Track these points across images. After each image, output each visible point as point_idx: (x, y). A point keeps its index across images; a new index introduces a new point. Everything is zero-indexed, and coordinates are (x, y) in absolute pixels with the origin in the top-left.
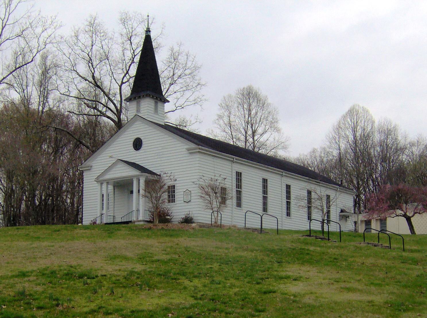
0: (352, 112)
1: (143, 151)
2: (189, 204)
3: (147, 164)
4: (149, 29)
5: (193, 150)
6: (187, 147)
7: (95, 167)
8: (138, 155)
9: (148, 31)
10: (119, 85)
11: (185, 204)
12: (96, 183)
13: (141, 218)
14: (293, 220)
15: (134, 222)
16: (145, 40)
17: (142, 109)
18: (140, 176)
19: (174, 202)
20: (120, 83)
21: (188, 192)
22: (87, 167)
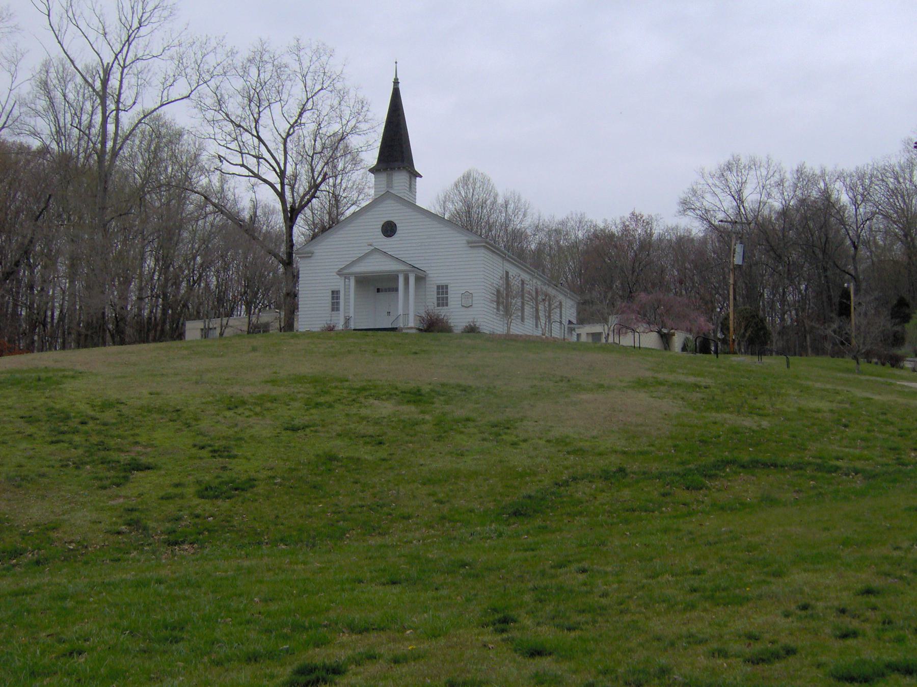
0: (466, 180)
1: (398, 239)
2: (470, 309)
3: (404, 256)
4: (398, 79)
5: (475, 243)
6: (467, 238)
7: (317, 254)
8: (388, 243)
9: (396, 82)
10: (282, 138)
11: (464, 309)
12: (338, 277)
13: (411, 324)
14: (526, 326)
15: (402, 329)
16: (393, 94)
17: (396, 185)
18: (410, 271)
19: (447, 305)
20: (284, 135)
21: (468, 295)
22: (305, 254)
